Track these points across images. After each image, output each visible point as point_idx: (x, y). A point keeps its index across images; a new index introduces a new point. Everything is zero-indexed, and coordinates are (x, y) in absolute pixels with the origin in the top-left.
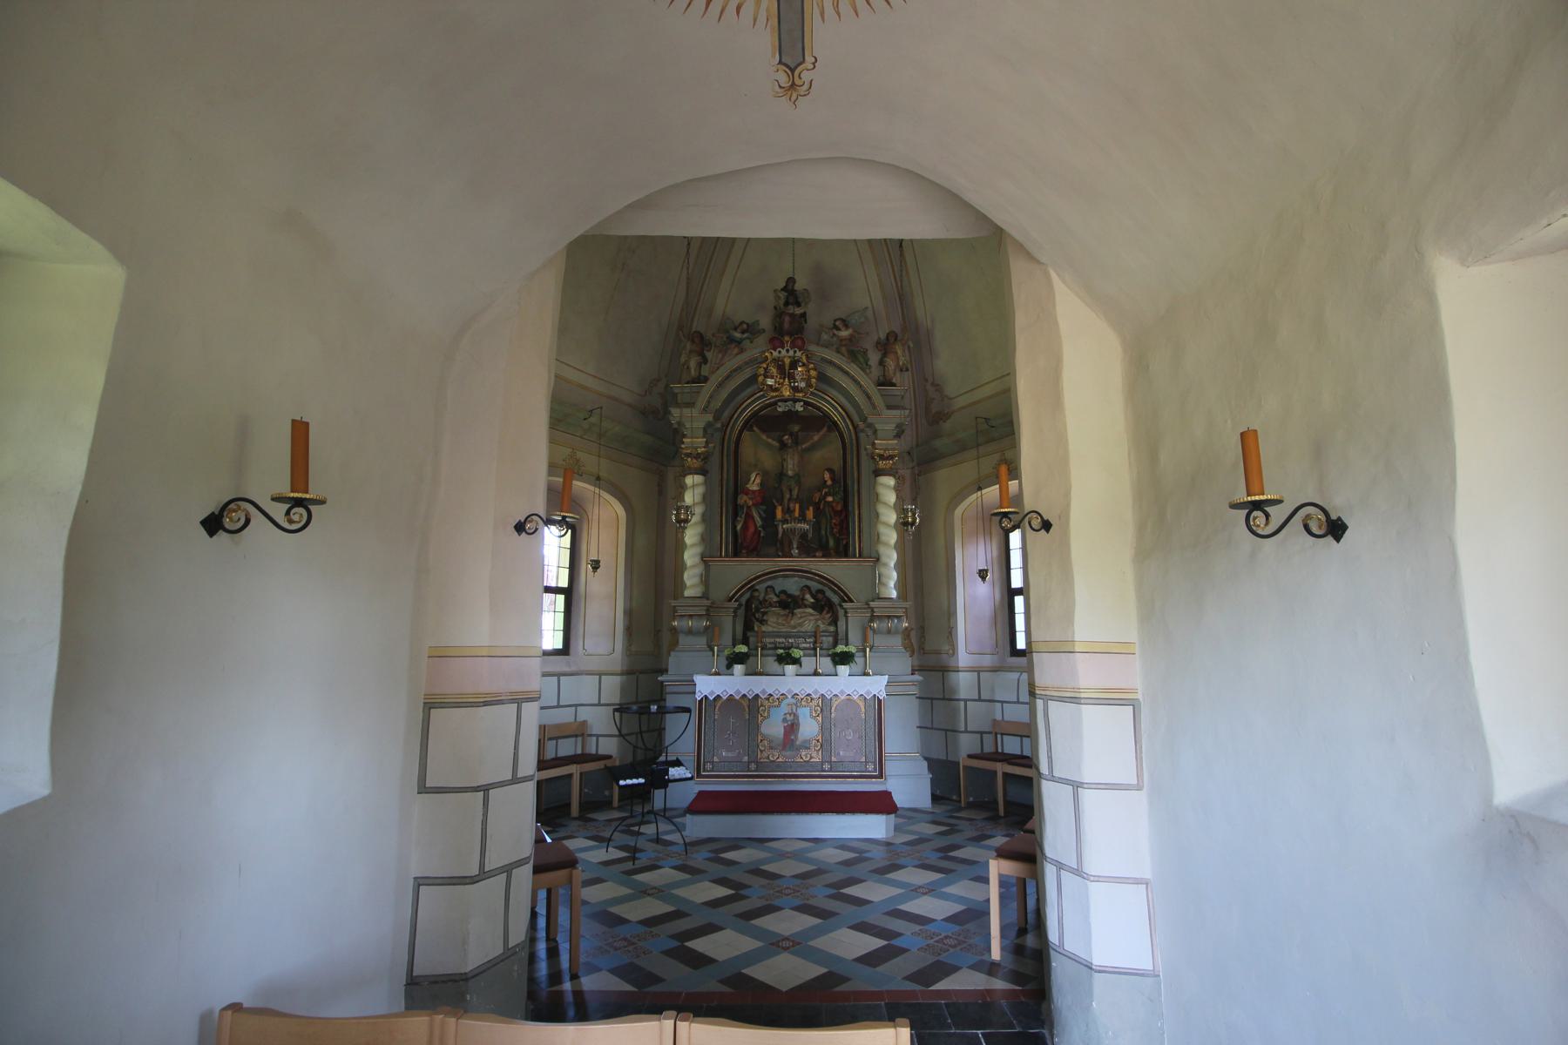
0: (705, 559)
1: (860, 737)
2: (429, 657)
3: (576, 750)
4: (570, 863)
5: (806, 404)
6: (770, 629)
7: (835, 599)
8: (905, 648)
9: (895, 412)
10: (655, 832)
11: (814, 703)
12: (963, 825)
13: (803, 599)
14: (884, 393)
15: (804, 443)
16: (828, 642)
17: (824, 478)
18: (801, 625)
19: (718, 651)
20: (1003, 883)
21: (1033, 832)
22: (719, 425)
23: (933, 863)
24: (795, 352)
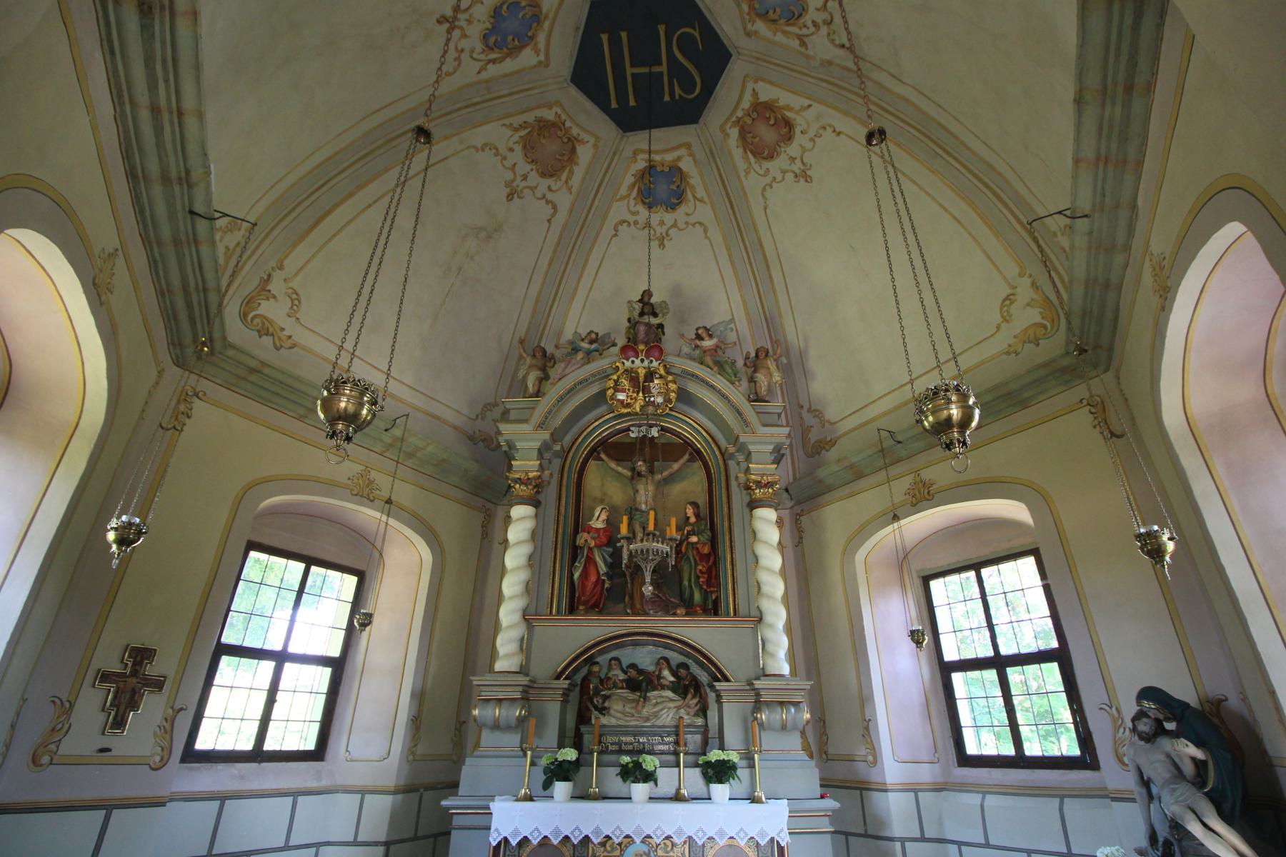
0: (529, 617)
5: (663, 429)
6: (613, 721)
7: (703, 677)
13: (659, 677)
14: (757, 410)
16: (695, 742)
17: (686, 514)
18: (656, 715)
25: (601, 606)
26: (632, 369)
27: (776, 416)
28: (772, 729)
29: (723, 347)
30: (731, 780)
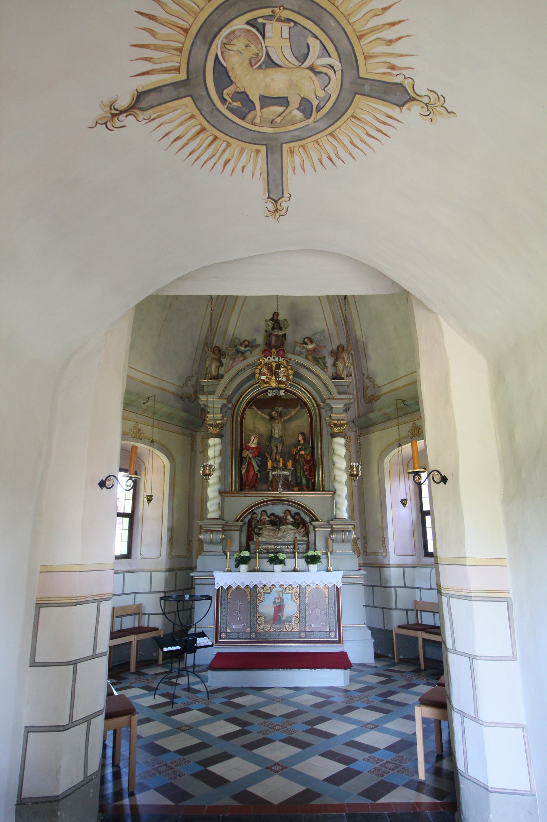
0: (221, 493)
1: (325, 614)
2: (40, 572)
3: (134, 624)
4: (130, 711)
5: (287, 391)
6: (264, 539)
7: (307, 519)
8: (354, 552)
9: (345, 396)
10: (188, 683)
11: (294, 590)
12: (396, 676)
13: (286, 519)
14: (336, 384)
15: (285, 416)
17: (299, 439)
18: (284, 537)
19: (230, 555)
20: (425, 721)
21: (443, 685)
22: (230, 406)
23: (377, 706)
24: (279, 358)
25: (256, 486)
26: (269, 362)
27: (346, 387)
28: (338, 542)
29: (318, 349)
30: (318, 563)
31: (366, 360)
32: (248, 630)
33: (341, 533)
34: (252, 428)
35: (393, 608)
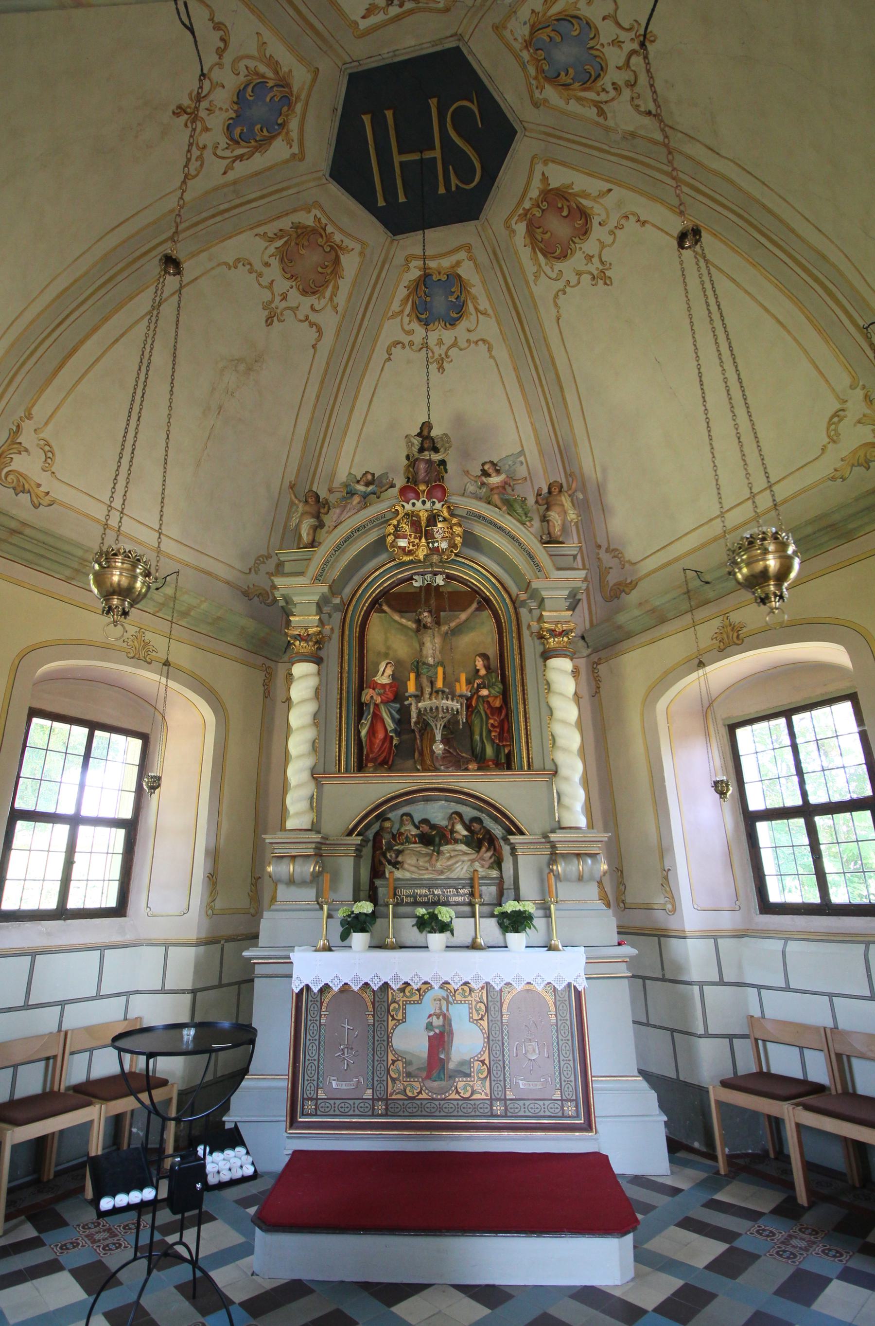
0: (317, 776)
5: (449, 577)
6: (408, 875)
7: (497, 831)
11: (475, 996)
13: (452, 831)
14: (550, 553)
16: (490, 894)
17: (476, 666)
18: (450, 868)
25: (390, 762)
26: (413, 512)
28: (568, 880)
31: (604, 514)
32: (368, 1094)
33: (575, 861)
34: (383, 649)
35: (699, 1033)
